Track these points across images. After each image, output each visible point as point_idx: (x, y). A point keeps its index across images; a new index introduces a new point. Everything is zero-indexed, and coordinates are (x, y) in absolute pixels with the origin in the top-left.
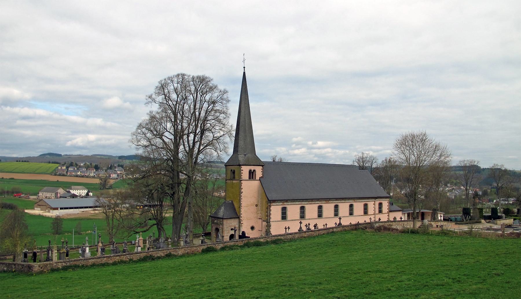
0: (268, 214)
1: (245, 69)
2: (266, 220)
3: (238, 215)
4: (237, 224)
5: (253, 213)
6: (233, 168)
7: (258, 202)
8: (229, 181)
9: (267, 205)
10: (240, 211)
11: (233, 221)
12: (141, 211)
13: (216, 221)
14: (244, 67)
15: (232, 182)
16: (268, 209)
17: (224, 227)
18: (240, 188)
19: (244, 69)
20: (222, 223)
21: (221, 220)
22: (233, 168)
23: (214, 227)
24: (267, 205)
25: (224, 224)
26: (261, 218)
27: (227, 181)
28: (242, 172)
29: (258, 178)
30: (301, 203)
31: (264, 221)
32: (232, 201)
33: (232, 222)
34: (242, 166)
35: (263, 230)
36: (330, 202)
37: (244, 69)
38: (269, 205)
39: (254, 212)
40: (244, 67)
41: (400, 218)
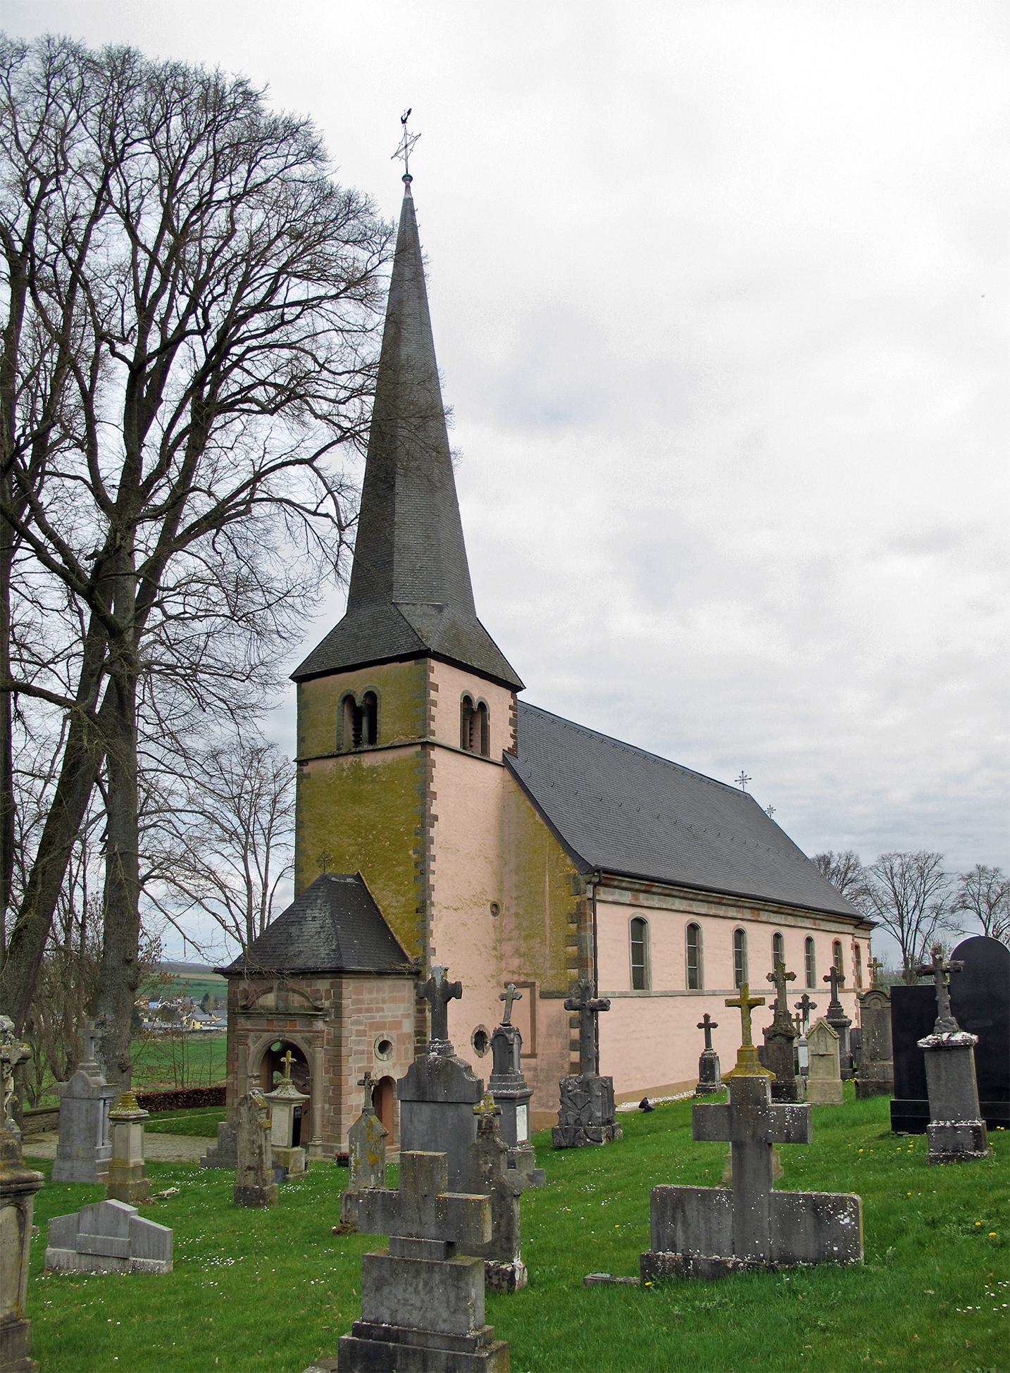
0: (581, 950)
1: (412, 184)
2: (563, 987)
3: (412, 959)
4: (407, 1016)
5: (482, 949)
6: (358, 683)
7: (500, 887)
8: (331, 763)
9: (578, 899)
10: (423, 934)
11: (386, 995)
12: (225, 106)
13: (270, 1000)
14: (407, 178)
15: (358, 766)
16: (582, 917)
17: (345, 1033)
18: (424, 795)
19: (408, 187)
20: (326, 1004)
21: (323, 985)
22: (358, 683)
23: (250, 1042)
24: (578, 899)
25: (346, 1013)
26: (522, 979)
27: (306, 769)
28: (433, 694)
29: (496, 754)
30: (688, 909)
31: (546, 995)
32: (358, 878)
33: (384, 1002)
34: (433, 663)
35: (539, 1051)
36: (764, 916)
37: (408, 187)
38: (590, 895)
39: (485, 946)
40: (407, 178)
41: (700, 1026)
